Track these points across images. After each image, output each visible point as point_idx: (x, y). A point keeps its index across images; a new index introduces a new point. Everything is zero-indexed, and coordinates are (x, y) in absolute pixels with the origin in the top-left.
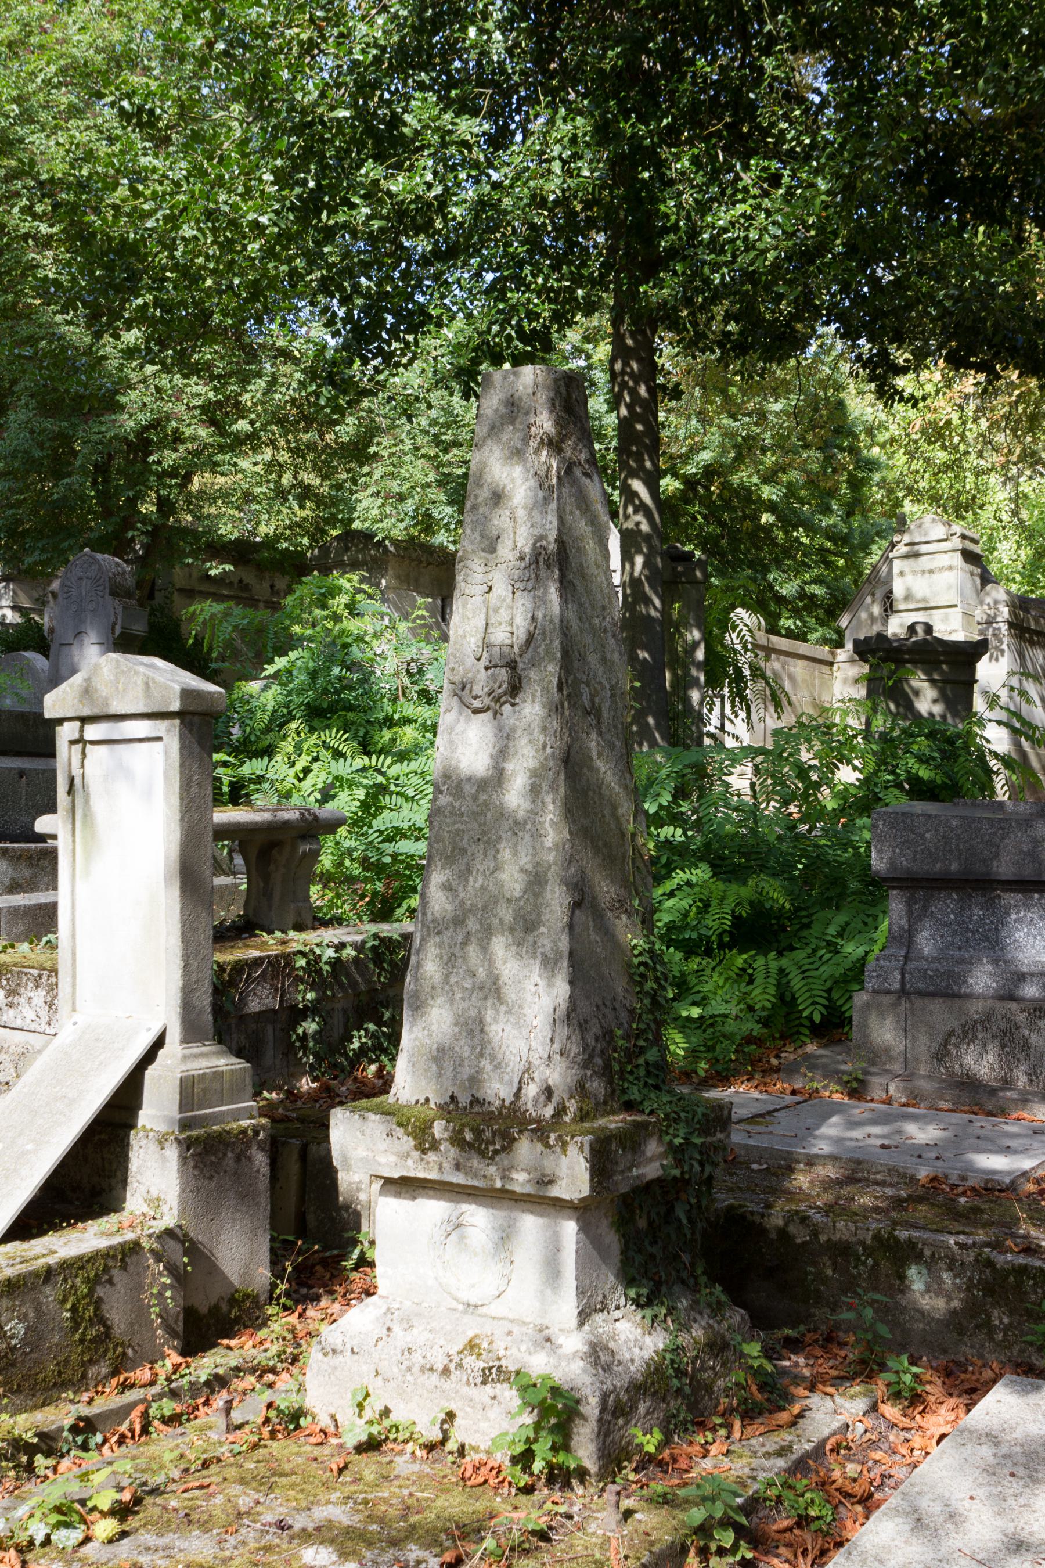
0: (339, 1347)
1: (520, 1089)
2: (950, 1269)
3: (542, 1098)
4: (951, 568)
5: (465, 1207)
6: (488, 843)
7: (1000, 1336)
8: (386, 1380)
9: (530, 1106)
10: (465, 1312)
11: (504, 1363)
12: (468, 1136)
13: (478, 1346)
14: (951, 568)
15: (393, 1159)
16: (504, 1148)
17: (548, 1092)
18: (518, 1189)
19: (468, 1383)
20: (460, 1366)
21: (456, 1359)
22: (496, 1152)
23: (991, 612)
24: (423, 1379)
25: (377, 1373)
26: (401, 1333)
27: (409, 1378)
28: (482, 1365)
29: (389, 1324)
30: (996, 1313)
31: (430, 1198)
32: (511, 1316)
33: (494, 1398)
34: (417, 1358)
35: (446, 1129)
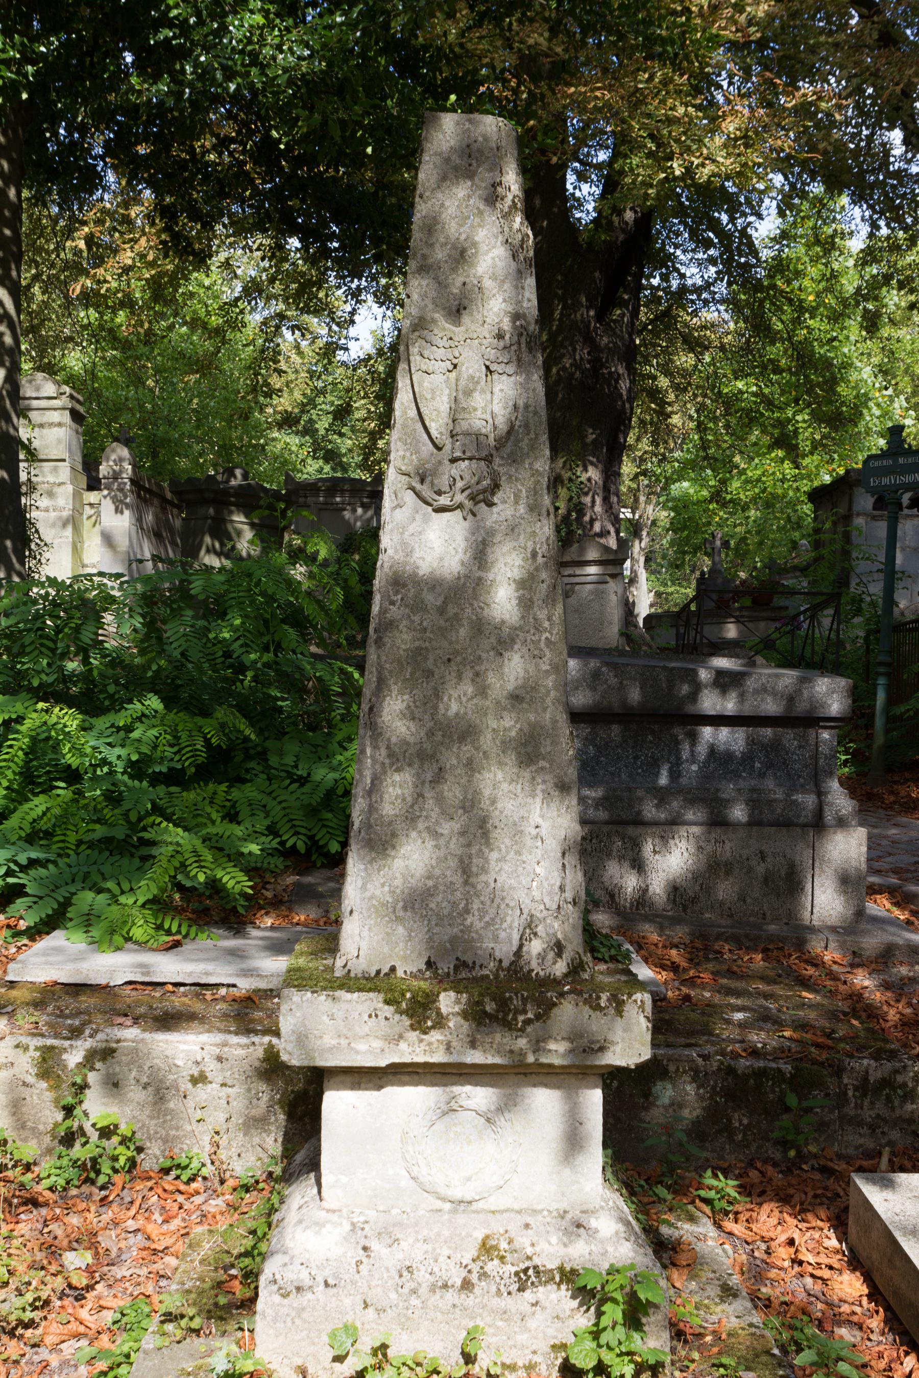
0: (307, 1282)
1: (521, 946)
2: (694, 1080)
3: (551, 955)
4: (60, 425)
5: (457, 1089)
6: (464, 662)
7: (740, 1137)
8: (380, 1311)
9: (534, 964)
10: (454, 1211)
11: (537, 1261)
12: (490, 1007)
13: (496, 1248)
14: (60, 425)
15: (377, 1044)
16: (538, 1017)
17: (559, 948)
18: (557, 1061)
19: (499, 1293)
20: (484, 1275)
21: (475, 1268)
22: (528, 1022)
23: (117, 468)
24: (435, 1299)
25: (366, 1305)
26: (385, 1251)
27: (414, 1301)
28: (514, 1269)
29: (363, 1242)
30: (736, 1116)
31: (404, 1084)
32: (516, 1207)
33: (536, 1304)
34: (422, 1276)
35: (457, 1001)
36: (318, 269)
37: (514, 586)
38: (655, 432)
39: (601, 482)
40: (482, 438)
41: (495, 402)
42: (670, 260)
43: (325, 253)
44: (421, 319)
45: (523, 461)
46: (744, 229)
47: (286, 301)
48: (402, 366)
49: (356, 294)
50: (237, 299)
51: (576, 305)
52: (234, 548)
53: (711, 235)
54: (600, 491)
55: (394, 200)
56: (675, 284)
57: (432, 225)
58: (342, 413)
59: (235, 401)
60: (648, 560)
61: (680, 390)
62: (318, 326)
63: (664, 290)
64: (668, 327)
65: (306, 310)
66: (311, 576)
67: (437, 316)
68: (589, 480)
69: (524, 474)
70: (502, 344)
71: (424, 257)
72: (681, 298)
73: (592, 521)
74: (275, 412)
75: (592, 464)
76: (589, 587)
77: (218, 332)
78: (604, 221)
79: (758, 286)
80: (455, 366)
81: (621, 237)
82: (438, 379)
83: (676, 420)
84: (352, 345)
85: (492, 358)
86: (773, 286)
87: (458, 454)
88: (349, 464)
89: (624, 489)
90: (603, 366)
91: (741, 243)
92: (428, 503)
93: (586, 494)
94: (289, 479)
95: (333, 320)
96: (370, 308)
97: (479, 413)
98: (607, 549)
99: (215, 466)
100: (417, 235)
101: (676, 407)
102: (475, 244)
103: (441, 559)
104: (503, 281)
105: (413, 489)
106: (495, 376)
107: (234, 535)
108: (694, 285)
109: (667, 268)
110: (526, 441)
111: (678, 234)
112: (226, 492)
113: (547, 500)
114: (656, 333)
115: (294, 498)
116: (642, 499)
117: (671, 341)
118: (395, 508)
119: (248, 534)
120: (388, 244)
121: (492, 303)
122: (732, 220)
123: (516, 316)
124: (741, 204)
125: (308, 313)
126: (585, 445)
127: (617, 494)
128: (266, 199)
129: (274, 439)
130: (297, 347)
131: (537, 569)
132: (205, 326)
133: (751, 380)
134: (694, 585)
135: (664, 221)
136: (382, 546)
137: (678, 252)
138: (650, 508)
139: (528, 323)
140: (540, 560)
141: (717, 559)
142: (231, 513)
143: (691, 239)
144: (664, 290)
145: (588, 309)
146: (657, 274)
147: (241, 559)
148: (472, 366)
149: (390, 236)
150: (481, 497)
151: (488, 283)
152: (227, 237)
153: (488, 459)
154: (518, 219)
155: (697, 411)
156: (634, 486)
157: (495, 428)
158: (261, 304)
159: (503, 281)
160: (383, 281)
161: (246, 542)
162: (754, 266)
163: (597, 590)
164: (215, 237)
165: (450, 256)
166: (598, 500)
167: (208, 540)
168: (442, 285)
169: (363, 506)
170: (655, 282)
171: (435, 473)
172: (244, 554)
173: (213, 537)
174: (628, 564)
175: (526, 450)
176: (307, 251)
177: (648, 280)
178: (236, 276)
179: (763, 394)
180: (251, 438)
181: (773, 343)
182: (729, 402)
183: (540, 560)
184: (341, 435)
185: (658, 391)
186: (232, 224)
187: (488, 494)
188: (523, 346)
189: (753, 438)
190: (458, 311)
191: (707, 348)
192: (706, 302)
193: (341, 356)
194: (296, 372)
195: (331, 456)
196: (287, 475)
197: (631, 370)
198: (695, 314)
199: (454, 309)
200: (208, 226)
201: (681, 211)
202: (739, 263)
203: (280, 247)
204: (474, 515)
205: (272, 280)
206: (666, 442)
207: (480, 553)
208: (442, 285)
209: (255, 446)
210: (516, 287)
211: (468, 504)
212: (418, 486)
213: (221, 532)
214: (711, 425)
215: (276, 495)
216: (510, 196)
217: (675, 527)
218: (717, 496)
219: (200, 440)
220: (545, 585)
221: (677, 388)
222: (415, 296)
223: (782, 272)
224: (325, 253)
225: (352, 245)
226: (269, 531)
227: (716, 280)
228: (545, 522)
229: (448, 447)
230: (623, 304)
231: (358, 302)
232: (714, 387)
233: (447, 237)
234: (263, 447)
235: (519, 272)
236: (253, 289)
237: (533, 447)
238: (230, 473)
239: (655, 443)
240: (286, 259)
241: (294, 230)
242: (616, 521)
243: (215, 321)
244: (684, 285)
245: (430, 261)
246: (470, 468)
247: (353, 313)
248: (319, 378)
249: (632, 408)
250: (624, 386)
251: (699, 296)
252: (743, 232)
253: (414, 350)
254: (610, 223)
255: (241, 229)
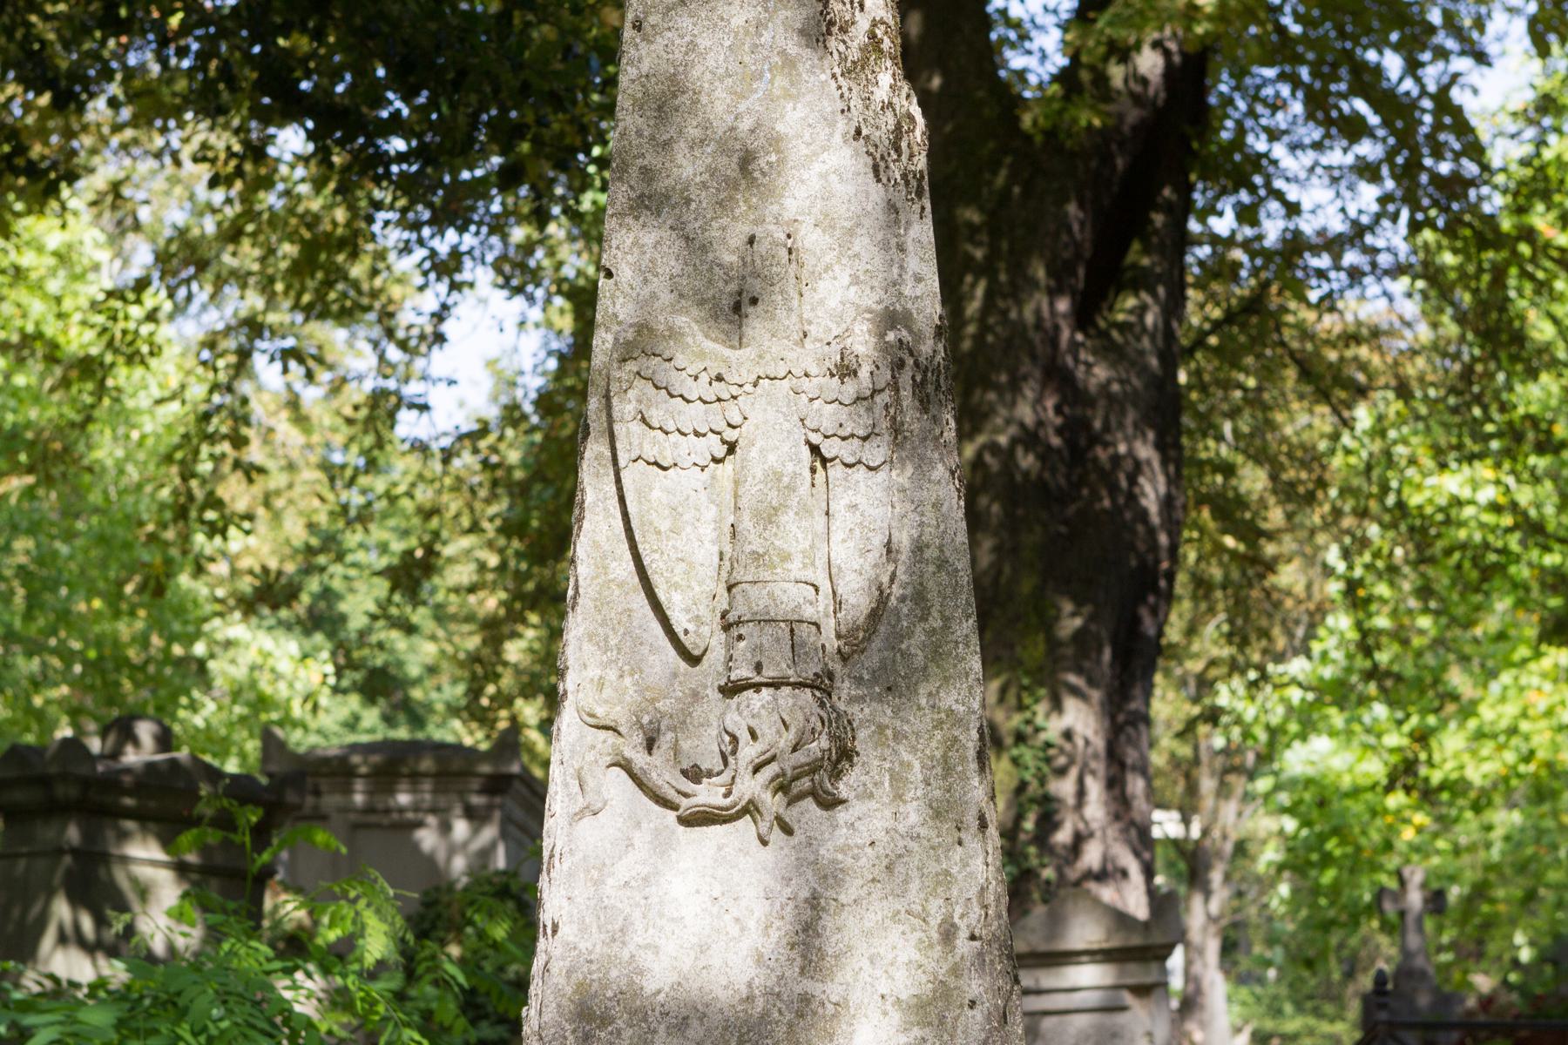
36: (352, 208)
37: (896, 1017)
38: (1240, 607)
39: (1099, 743)
40: (804, 631)
41: (837, 537)
42: (1258, 168)
43: (372, 165)
44: (643, 328)
45: (913, 689)
46: (1444, 90)
47: (266, 286)
48: (595, 449)
49: (446, 268)
50: (141, 285)
51: (1020, 286)
52: (130, 930)
53: (1361, 105)
54: (1100, 766)
55: (547, 31)
56: (1273, 229)
57: (667, 101)
58: (410, 575)
59: (127, 546)
60: (1229, 948)
61: (1297, 497)
62: (352, 351)
63: (1246, 245)
64: (1258, 341)
65: (318, 310)
66: (338, 1000)
67: (681, 321)
68: (1068, 735)
69: (917, 722)
70: (850, 389)
71: (647, 174)
72: (1290, 265)
73: (1079, 840)
74: (235, 573)
75: (1075, 692)
76: (1081, 1021)
77: (89, 367)
78: (1085, 76)
79: (1487, 235)
80: (732, 448)
81: (1133, 115)
82: (687, 481)
83: (1289, 576)
84: (437, 396)
85: (828, 426)
86: (1529, 234)
87: (743, 672)
88: (429, 707)
89: (1158, 759)
90: (1095, 439)
91: (1438, 126)
92: (672, 806)
93: (1061, 772)
94: (272, 745)
95: (390, 333)
96: (483, 301)
97: (795, 568)
98: (1121, 919)
99: (75, 713)
100: (628, 122)
101: (1288, 544)
102: (776, 142)
103: (703, 949)
104: (851, 232)
105: (626, 766)
106: (836, 471)
107: (131, 896)
108: (1322, 232)
109: (1252, 189)
110: (919, 636)
111: (1276, 106)
112: (112, 783)
113: (977, 790)
114: (1229, 356)
115: (291, 797)
116: (1207, 784)
117: (1268, 373)
118: (579, 815)
119: (168, 890)
120: (537, 142)
121: (823, 286)
122: (1413, 67)
123: (891, 319)
124: (1432, 30)
125: (323, 315)
126: (1053, 644)
127: (1143, 769)
128: (223, 33)
129: (229, 644)
130: (294, 403)
131: (955, 971)
132: (53, 355)
133: (1484, 470)
134: (1354, 1009)
135: (1240, 73)
136: (546, 916)
137: (1279, 151)
138: (1229, 810)
139: (918, 337)
140: (963, 946)
141: (1413, 941)
142: (124, 836)
143: (1310, 116)
144: (1246, 245)
145: (1053, 293)
146: (1227, 205)
147: (151, 958)
148: (774, 445)
149: (542, 122)
150: (805, 784)
151: (811, 239)
152: (117, 128)
153: (821, 685)
154: (885, 79)
155: (1346, 554)
156: (1185, 751)
157: (838, 604)
158: (202, 294)
159: (851, 232)
160: (518, 234)
161: (164, 916)
162: (1472, 183)
163: (1099, 1029)
164: (85, 128)
165: (713, 171)
166: (1095, 788)
167: (62, 910)
168: (695, 246)
169: (471, 814)
170: (1223, 224)
171: (681, 723)
172: (159, 947)
173: (76, 901)
174: (1176, 960)
175: (920, 659)
176: (326, 162)
177: (1202, 220)
178: (137, 227)
179: (1514, 506)
180: (171, 639)
181: (1532, 374)
182: (1423, 533)
183: (963, 946)
184: (410, 629)
185: (1241, 502)
186: (132, 97)
187: (823, 776)
188: (906, 393)
189: (1489, 624)
190: (737, 308)
191: (1362, 392)
192: (1355, 275)
193: (408, 425)
194: (291, 467)
195: (380, 684)
196: (267, 737)
197: (1169, 448)
198: (1328, 304)
199: (726, 302)
200: (68, 100)
201: (1281, 50)
202: (1436, 178)
203: (256, 151)
204: (788, 830)
205: (232, 234)
206: (1265, 634)
207: (808, 937)
208: (695, 246)
209: (180, 663)
210: (885, 246)
211: (773, 803)
212: (639, 759)
213: (98, 889)
214: (1382, 589)
215: (241, 788)
216: (863, 24)
217: (1298, 863)
218: (1404, 773)
219: (33, 648)
220: (978, 1014)
221: (1286, 492)
222: (625, 273)
223: (1546, 196)
224: (372, 165)
225: (442, 150)
226: (226, 887)
227: (1377, 218)
228: (973, 844)
229: (715, 657)
230: (1143, 280)
231: (455, 287)
232: (1385, 489)
233: (706, 126)
234: (201, 664)
235: (892, 208)
236: (184, 259)
237: (937, 652)
238: (123, 730)
239: (1238, 637)
240: (267, 183)
241: (290, 108)
242: (1141, 839)
243: (79, 340)
244: (1297, 233)
245: (661, 185)
246: (775, 707)
247: (440, 316)
248: (351, 483)
249: (1173, 549)
250: (1151, 492)
251: (1337, 258)
252: (1442, 100)
253: (625, 408)
254: (1101, 79)
255: (150, 106)
